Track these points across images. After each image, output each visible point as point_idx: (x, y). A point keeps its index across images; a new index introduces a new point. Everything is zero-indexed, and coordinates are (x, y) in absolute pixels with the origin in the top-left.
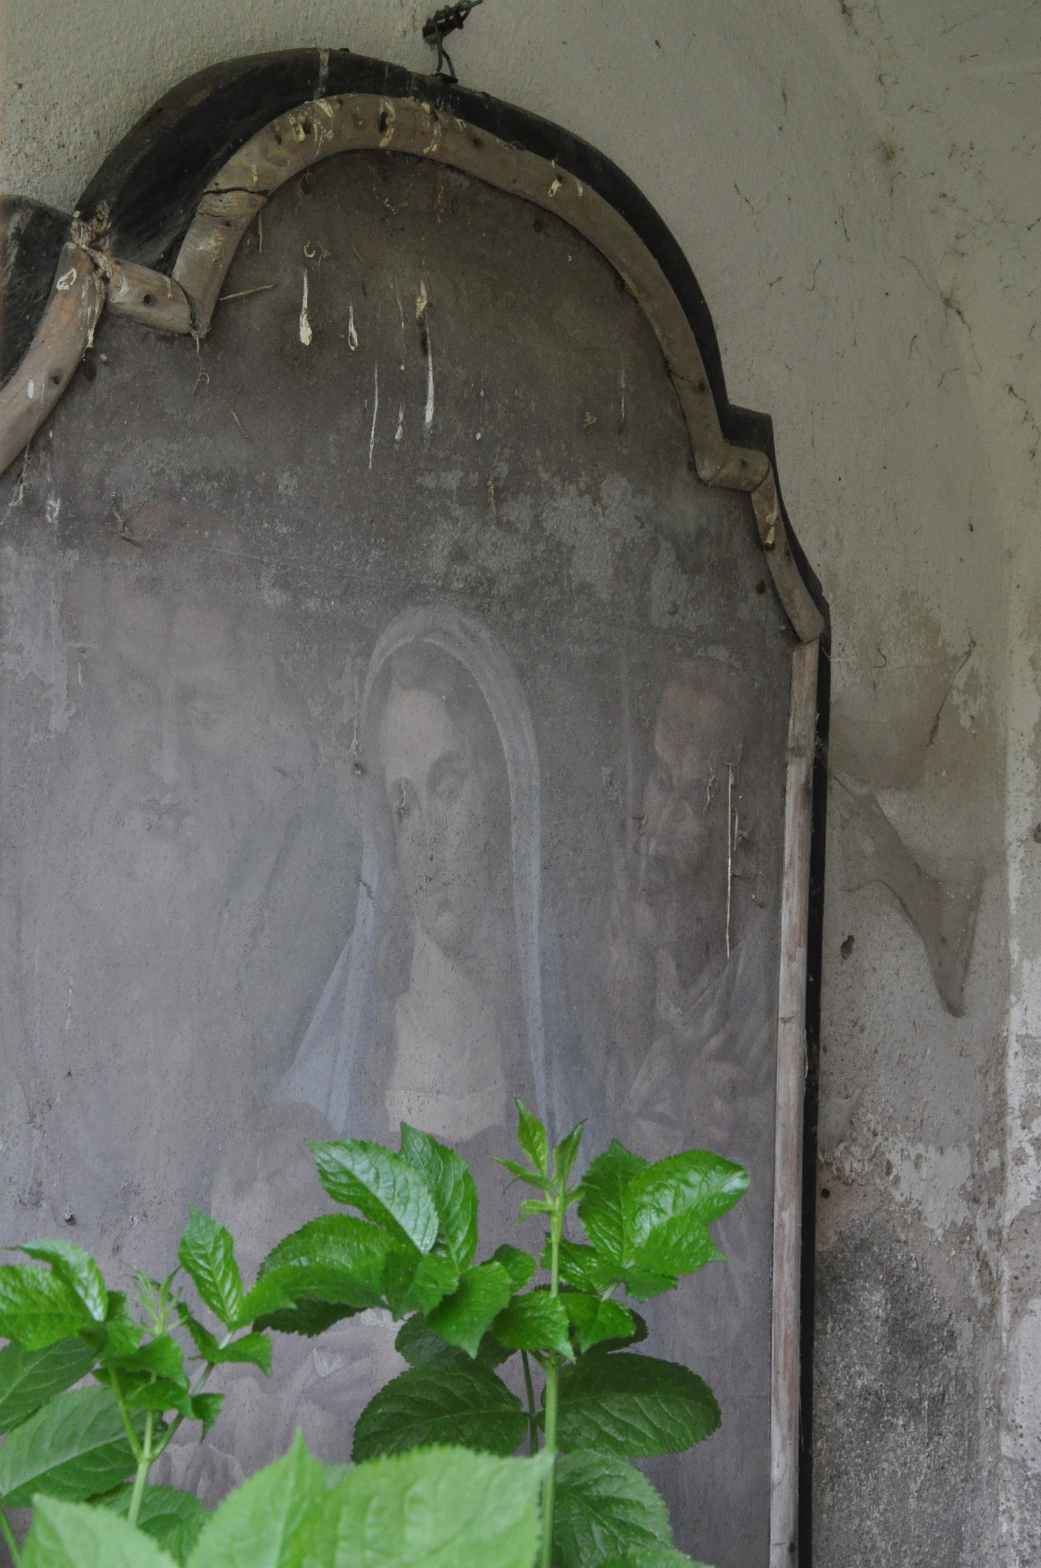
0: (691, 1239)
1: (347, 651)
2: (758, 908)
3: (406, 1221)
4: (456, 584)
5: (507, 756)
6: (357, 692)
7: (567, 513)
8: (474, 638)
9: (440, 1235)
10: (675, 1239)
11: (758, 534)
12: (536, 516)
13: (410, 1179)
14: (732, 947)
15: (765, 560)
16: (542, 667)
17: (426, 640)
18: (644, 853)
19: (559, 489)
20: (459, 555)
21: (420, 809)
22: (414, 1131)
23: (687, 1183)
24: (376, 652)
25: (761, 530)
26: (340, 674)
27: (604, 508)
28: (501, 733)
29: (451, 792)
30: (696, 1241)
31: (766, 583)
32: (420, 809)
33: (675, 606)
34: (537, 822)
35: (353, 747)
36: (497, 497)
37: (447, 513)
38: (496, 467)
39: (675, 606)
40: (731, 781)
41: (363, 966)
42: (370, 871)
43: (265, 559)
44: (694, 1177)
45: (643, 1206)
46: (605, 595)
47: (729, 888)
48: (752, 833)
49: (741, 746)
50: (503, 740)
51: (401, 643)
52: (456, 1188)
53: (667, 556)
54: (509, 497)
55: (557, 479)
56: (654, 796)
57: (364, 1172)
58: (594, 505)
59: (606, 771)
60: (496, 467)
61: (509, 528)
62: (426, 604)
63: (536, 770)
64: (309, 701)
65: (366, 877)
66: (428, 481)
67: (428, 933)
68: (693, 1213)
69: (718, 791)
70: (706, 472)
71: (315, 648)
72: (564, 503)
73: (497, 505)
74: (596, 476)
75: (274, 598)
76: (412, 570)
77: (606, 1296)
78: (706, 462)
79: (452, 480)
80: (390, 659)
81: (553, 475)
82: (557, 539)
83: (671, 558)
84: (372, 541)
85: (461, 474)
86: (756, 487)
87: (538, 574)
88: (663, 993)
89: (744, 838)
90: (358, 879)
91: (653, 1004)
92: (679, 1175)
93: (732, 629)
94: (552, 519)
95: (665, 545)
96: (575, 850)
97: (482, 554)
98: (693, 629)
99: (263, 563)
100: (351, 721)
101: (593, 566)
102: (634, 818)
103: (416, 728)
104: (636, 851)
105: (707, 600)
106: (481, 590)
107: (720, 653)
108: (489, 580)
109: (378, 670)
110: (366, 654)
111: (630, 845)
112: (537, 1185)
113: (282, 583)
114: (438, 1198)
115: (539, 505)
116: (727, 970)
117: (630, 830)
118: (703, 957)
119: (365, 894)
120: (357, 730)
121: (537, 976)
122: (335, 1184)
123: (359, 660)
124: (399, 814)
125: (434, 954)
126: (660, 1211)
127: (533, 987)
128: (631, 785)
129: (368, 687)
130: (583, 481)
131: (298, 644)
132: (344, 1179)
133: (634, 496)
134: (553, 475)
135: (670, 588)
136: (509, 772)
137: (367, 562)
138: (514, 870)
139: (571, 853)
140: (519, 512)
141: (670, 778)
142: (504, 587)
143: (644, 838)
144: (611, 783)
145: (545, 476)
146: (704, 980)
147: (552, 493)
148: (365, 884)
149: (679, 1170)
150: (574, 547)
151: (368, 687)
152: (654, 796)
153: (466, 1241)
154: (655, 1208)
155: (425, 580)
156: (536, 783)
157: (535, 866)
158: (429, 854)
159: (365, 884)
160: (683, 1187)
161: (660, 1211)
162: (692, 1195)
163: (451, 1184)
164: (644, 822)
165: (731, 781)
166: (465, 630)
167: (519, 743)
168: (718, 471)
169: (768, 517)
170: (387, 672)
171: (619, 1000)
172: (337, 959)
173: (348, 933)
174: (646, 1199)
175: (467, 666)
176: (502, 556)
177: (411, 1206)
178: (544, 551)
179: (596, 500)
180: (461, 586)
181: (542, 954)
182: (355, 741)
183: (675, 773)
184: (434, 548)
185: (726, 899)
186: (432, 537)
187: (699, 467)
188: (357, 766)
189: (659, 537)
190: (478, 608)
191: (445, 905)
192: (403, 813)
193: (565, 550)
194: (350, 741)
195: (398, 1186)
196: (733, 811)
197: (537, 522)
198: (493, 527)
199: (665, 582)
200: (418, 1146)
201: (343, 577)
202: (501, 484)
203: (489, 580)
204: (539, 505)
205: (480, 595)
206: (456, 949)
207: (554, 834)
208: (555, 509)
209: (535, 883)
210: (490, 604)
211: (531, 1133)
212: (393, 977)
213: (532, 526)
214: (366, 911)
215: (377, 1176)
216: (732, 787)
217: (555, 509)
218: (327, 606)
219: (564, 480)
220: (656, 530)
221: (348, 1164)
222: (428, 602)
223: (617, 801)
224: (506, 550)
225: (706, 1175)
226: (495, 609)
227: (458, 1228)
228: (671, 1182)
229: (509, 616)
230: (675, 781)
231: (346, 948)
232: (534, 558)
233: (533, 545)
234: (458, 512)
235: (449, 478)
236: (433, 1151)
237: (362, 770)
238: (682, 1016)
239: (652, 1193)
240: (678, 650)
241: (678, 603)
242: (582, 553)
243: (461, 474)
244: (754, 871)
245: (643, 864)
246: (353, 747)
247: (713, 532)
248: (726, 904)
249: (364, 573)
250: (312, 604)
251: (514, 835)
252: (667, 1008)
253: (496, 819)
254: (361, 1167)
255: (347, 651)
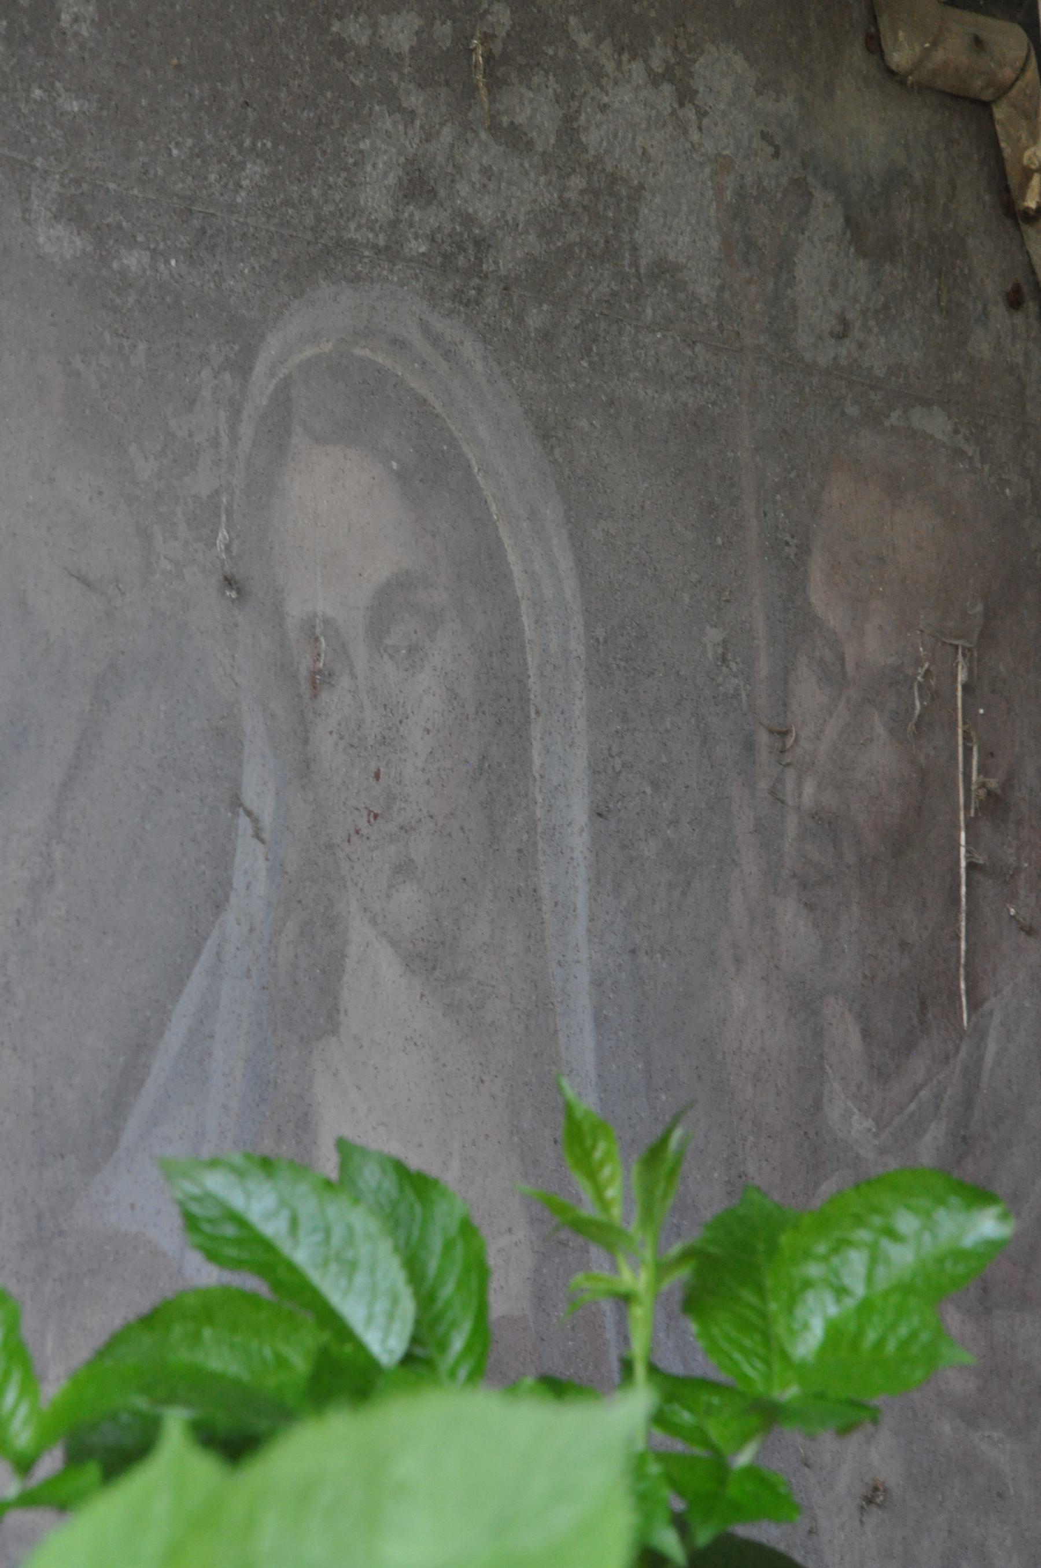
0: (903, 1331)
1: (204, 358)
2: (1023, 935)
3: (353, 1311)
4: (413, 244)
5: (520, 585)
6: (225, 440)
7: (626, 112)
8: (449, 354)
9: (415, 1340)
10: (871, 1336)
11: (1007, 189)
12: (569, 119)
13: (358, 1227)
14: (974, 1005)
15: (1023, 244)
16: (583, 423)
17: (358, 352)
18: (790, 801)
19: (610, 66)
20: (417, 186)
21: (354, 677)
22: (364, 1151)
23: (891, 1234)
24: (260, 368)
25: (1013, 182)
26: (193, 402)
27: (702, 114)
28: (507, 542)
29: (413, 649)
30: (913, 1335)
31: (1025, 289)
32: (354, 677)
33: (844, 322)
34: (582, 724)
35: (220, 545)
36: (490, 74)
37: (391, 98)
38: (487, 12)
39: (844, 322)
40: (961, 677)
41: (248, 974)
42: (259, 785)
43: (39, 162)
44: (906, 1222)
45: (807, 1284)
46: (704, 289)
47: (963, 890)
48: (1008, 784)
49: (979, 608)
50: (512, 557)
51: (309, 352)
52: (449, 1246)
53: (826, 217)
54: (514, 76)
55: (606, 47)
56: (808, 693)
57: (269, 1216)
58: (682, 105)
59: (714, 635)
60: (487, 12)
61: (515, 139)
62: (356, 279)
63: (577, 622)
64: (133, 449)
65: (249, 797)
66: (354, 30)
67: (373, 921)
68: (905, 1289)
69: (938, 697)
70: (901, 55)
71: (142, 346)
72: (624, 95)
73: (490, 92)
74: (683, 45)
75: (58, 242)
76: (328, 209)
77: (744, 1458)
78: (901, 34)
79: (401, 32)
80: (287, 383)
81: (599, 40)
82: (609, 168)
83: (836, 224)
84: (247, 143)
85: (417, 23)
86: (1003, 91)
87: (573, 236)
88: (836, 1085)
89: (989, 793)
90: (236, 802)
91: (817, 1106)
92: (877, 1220)
93: (958, 376)
94: (599, 126)
95: (822, 197)
96: (655, 784)
97: (463, 188)
98: (880, 372)
99: (34, 169)
100: (217, 493)
101: (681, 229)
102: (771, 732)
103: (340, 522)
104: (776, 794)
105: (907, 316)
106: (461, 261)
107: (935, 424)
108: (478, 243)
109: (265, 402)
110: (242, 367)
111: (763, 785)
112: (602, 1234)
113: (73, 212)
114: (414, 1268)
115: (573, 97)
116: (962, 1054)
117: (764, 756)
118: (915, 1021)
119: (250, 831)
120: (229, 513)
121: (589, 1026)
122: (213, 1238)
123: (227, 377)
124: (314, 685)
125: (387, 965)
126: (841, 1292)
127: (581, 1045)
128: (763, 667)
129: (246, 430)
130: (660, 55)
131: (107, 335)
132: (230, 1230)
133: (759, 93)
134: (599, 40)
135: (834, 284)
136: (525, 621)
137: (239, 186)
138: (539, 813)
139: (649, 790)
140: (534, 107)
141: (842, 660)
142: (508, 258)
143: (791, 775)
144: (724, 660)
145: (584, 40)
146: (918, 1066)
147: (598, 75)
148: (249, 813)
149: (875, 1210)
150: (641, 187)
151: (246, 430)
152: (808, 693)
153: (468, 1348)
154: (831, 1285)
155: (351, 233)
156: (577, 647)
157: (578, 811)
158: (373, 766)
159: (249, 813)
160: (885, 1243)
161: (841, 1292)
162: (902, 1257)
163: (437, 1244)
164: (790, 741)
165: (961, 677)
166: (435, 340)
167: (542, 566)
168: (926, 53)
169: (1027, 154)
170: (282, 400)
171: (750, 1089)
172: (197, 956)
173: (219, 907)
174: (814, 1270)
175: (439, 410)
176: (503, 196)
177: (361, 1278)
178: (582, 192)
179: (685, 95)
180: (423, 249)
181: (597, 983)
182: (223, 534)
183: (850, 652)
184: (369, 168)
185: (958, 912)
186: (365, 145)
187: (887, 43)
188: (229, 582)
189: (810, 179)
190: (457, 296)
191: (403, 869)
192: (319, 681)
193: (624, 192)
194: (215, 532)
195: (336, 1240)
196: (967, 737)
197: (569, 131)
198: (483, 136)
199: (823, 271)
200: (371, 1176)
201: (191, 212)
202: (497, 48)
203: (478, 243)
204: (573, 97)
205: (459, 266)
206: (429, 958)
207: (615, 750)
208: (604, 108)
209: (579, 842)
210: (479, 290)
211: (588, 1143)
212: (306, 1005)
213: (559, 139)
214: (251, 863)
215: (294, 1223)
216: (964, 687)
217: (604, 108)
218: (162, 267)
219: (620, 50)
220: (804, 165)
221: (237, 1200)
222: (358, 278)
223: (737, 695)
224: (510, 183)
225: (928, 1215)
226: (491, 301)
227: (454, 1324)
228: (863, 1235)
229: (519, 319)
230: (850, 667)
231: (215, 933)
232: (564, 204)
233: (560, 177)
234: (414, 100)
235: (395, 28)
236: (401, 1189)
237: (239, 591)
238: (876, 1136)
239: (825, 1258)
240: (852, 410)
241: (850, 316)
242: (658, 200)
243: (417, 23)
244: (1012, 860)
245: (792, 825)
246: (220, 545)
247: (917, 175)
248: (958, 921)
249: (232, 208)
250: (133, 260)
251: (537, 747)
252: (846, 1116)
253: (501, 708)
254: (260, 1205)
255: (204, 358)
